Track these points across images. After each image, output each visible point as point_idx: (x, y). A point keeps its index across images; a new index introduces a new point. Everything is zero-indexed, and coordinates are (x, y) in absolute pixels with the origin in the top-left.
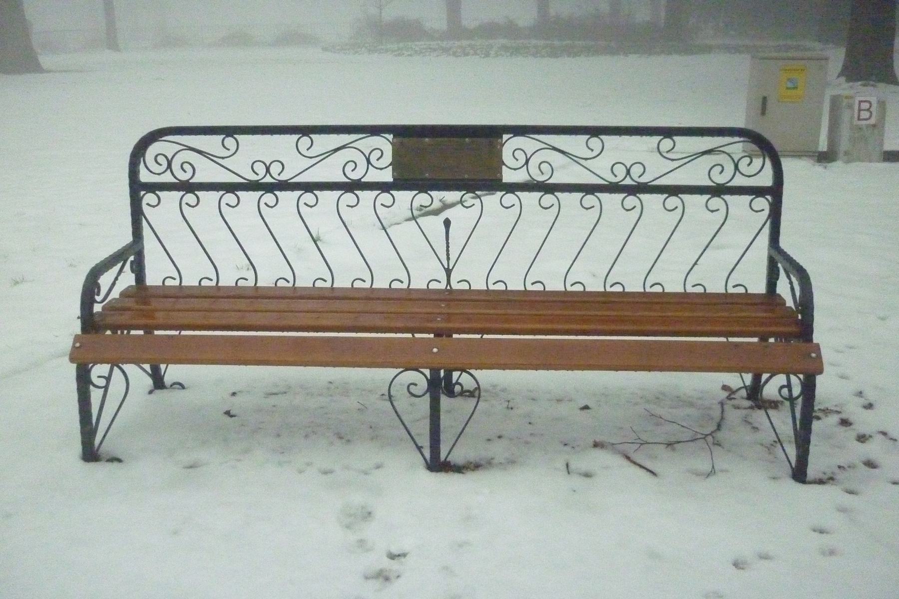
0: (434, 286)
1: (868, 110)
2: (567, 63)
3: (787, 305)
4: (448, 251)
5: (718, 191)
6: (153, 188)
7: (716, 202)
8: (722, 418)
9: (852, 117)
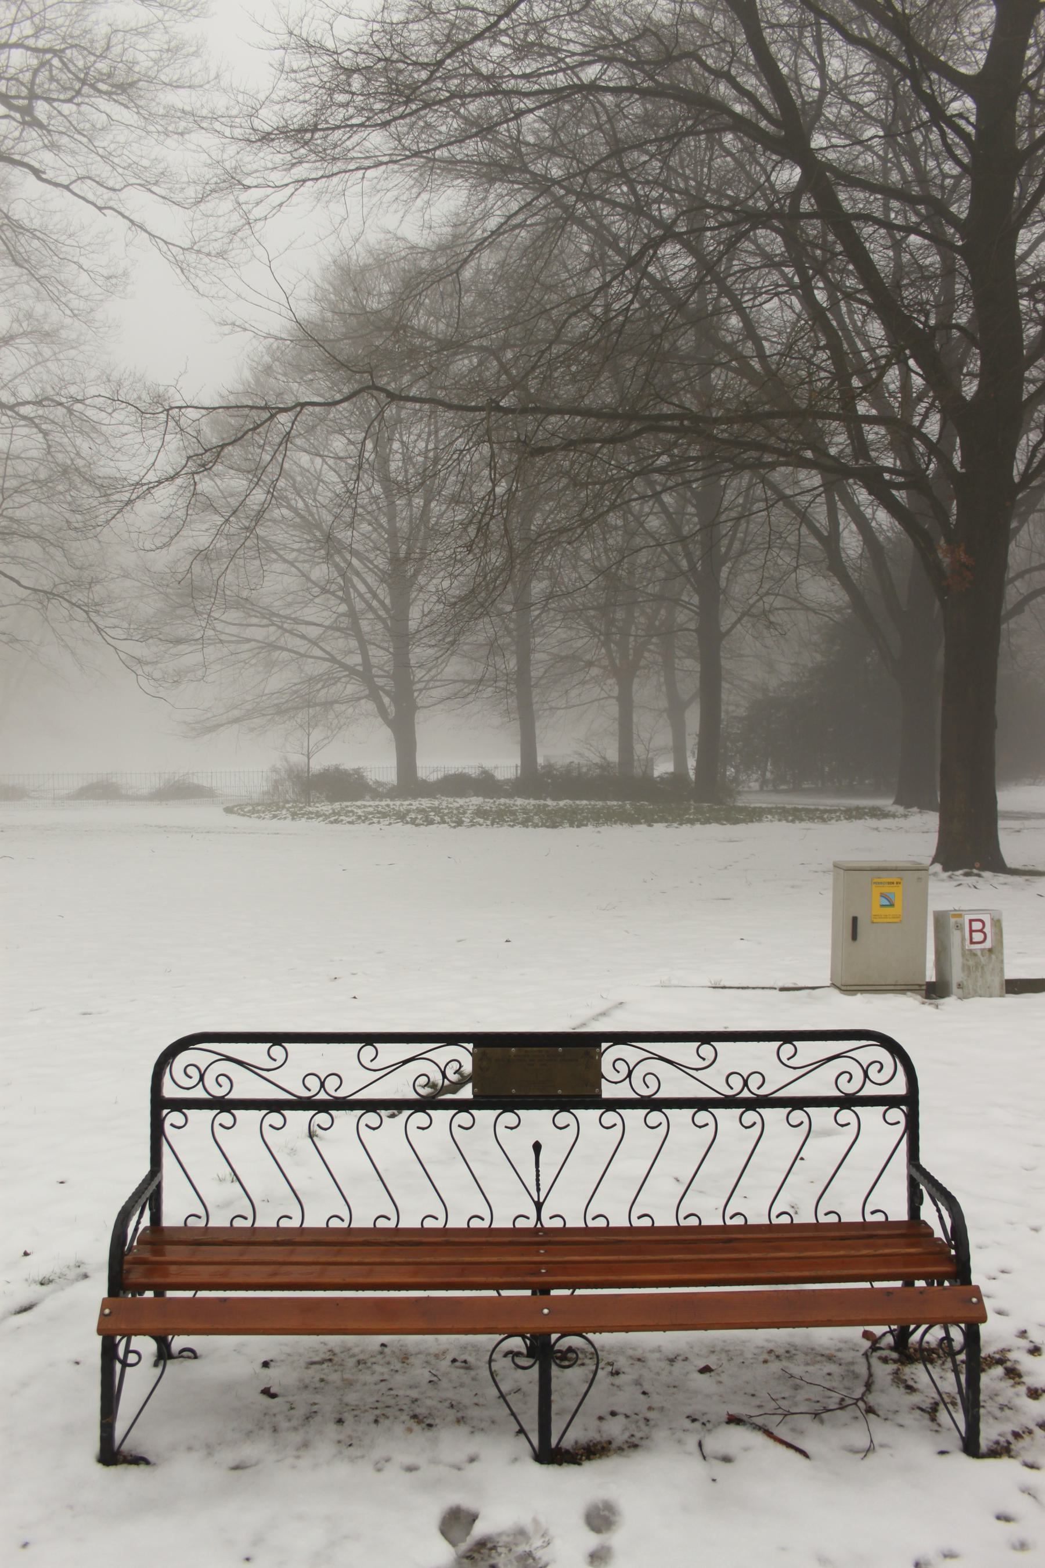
0: (521, 1224)
1: (981, 931)
2: (567, 836)
3: (936, 1236)
4: (538, 1180)
5: (847, 1102)
6: (180, 1105)
7: (846, 1115)
8: (870, 1375)
9: (963, 939)
